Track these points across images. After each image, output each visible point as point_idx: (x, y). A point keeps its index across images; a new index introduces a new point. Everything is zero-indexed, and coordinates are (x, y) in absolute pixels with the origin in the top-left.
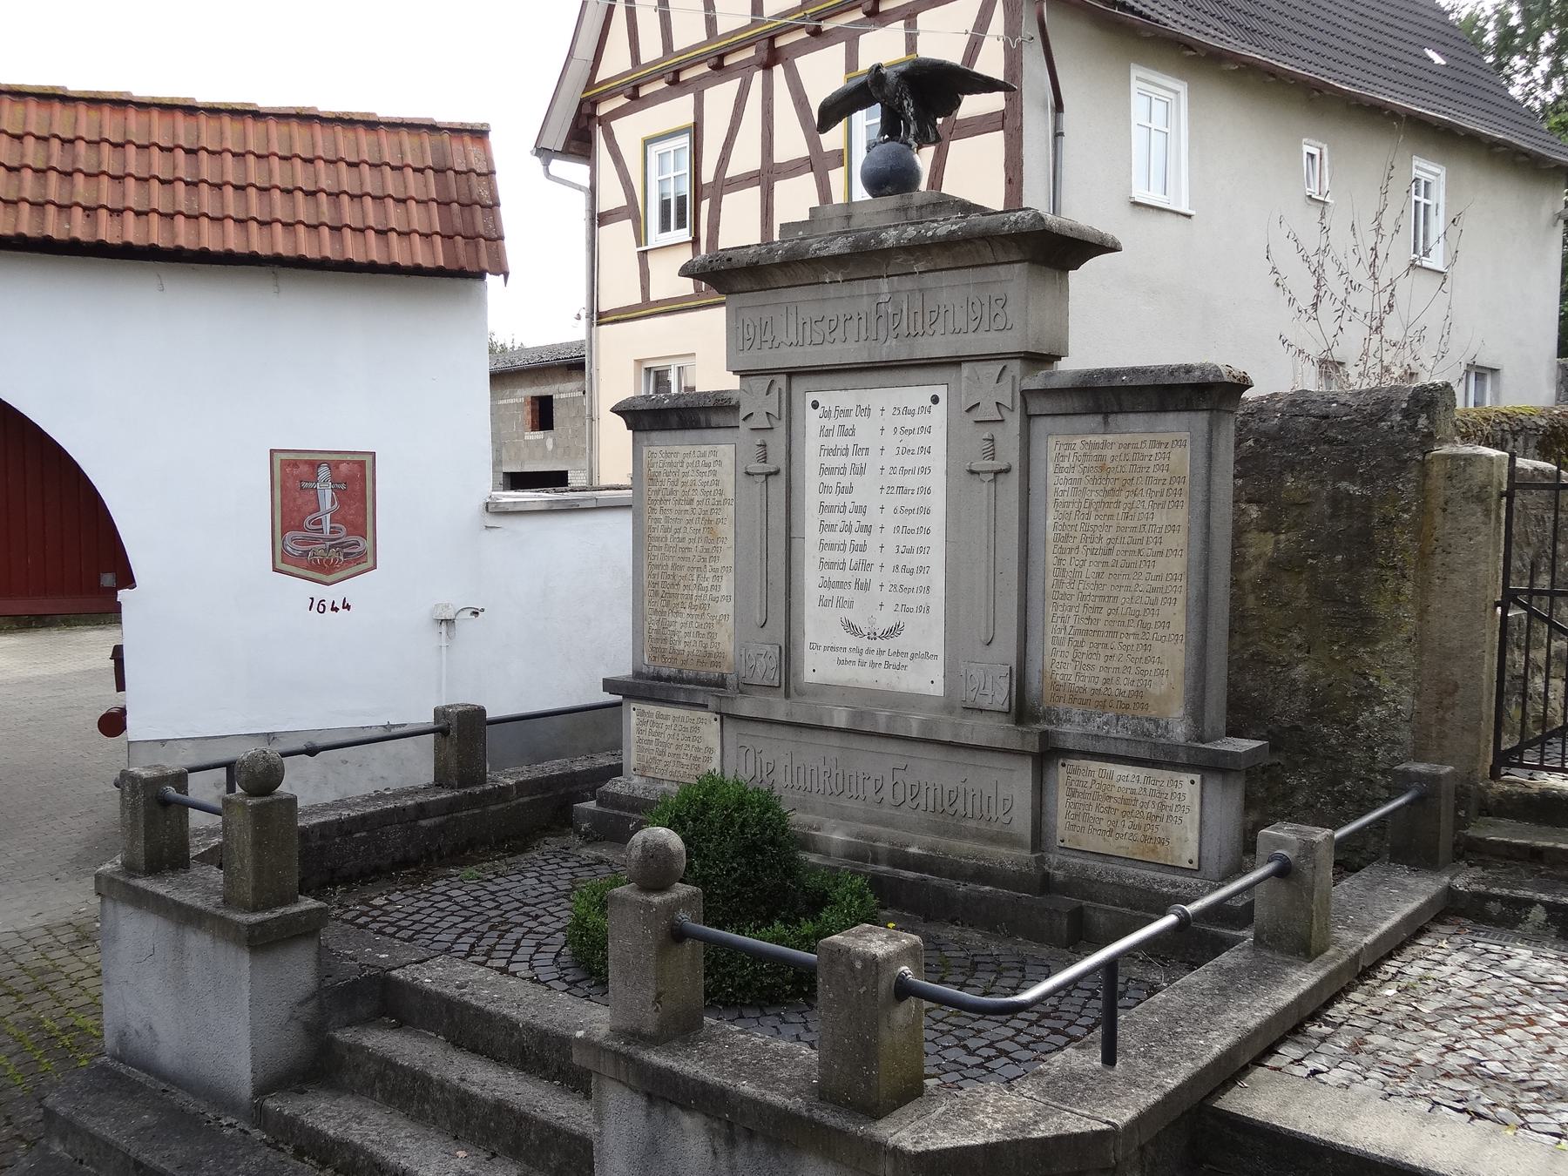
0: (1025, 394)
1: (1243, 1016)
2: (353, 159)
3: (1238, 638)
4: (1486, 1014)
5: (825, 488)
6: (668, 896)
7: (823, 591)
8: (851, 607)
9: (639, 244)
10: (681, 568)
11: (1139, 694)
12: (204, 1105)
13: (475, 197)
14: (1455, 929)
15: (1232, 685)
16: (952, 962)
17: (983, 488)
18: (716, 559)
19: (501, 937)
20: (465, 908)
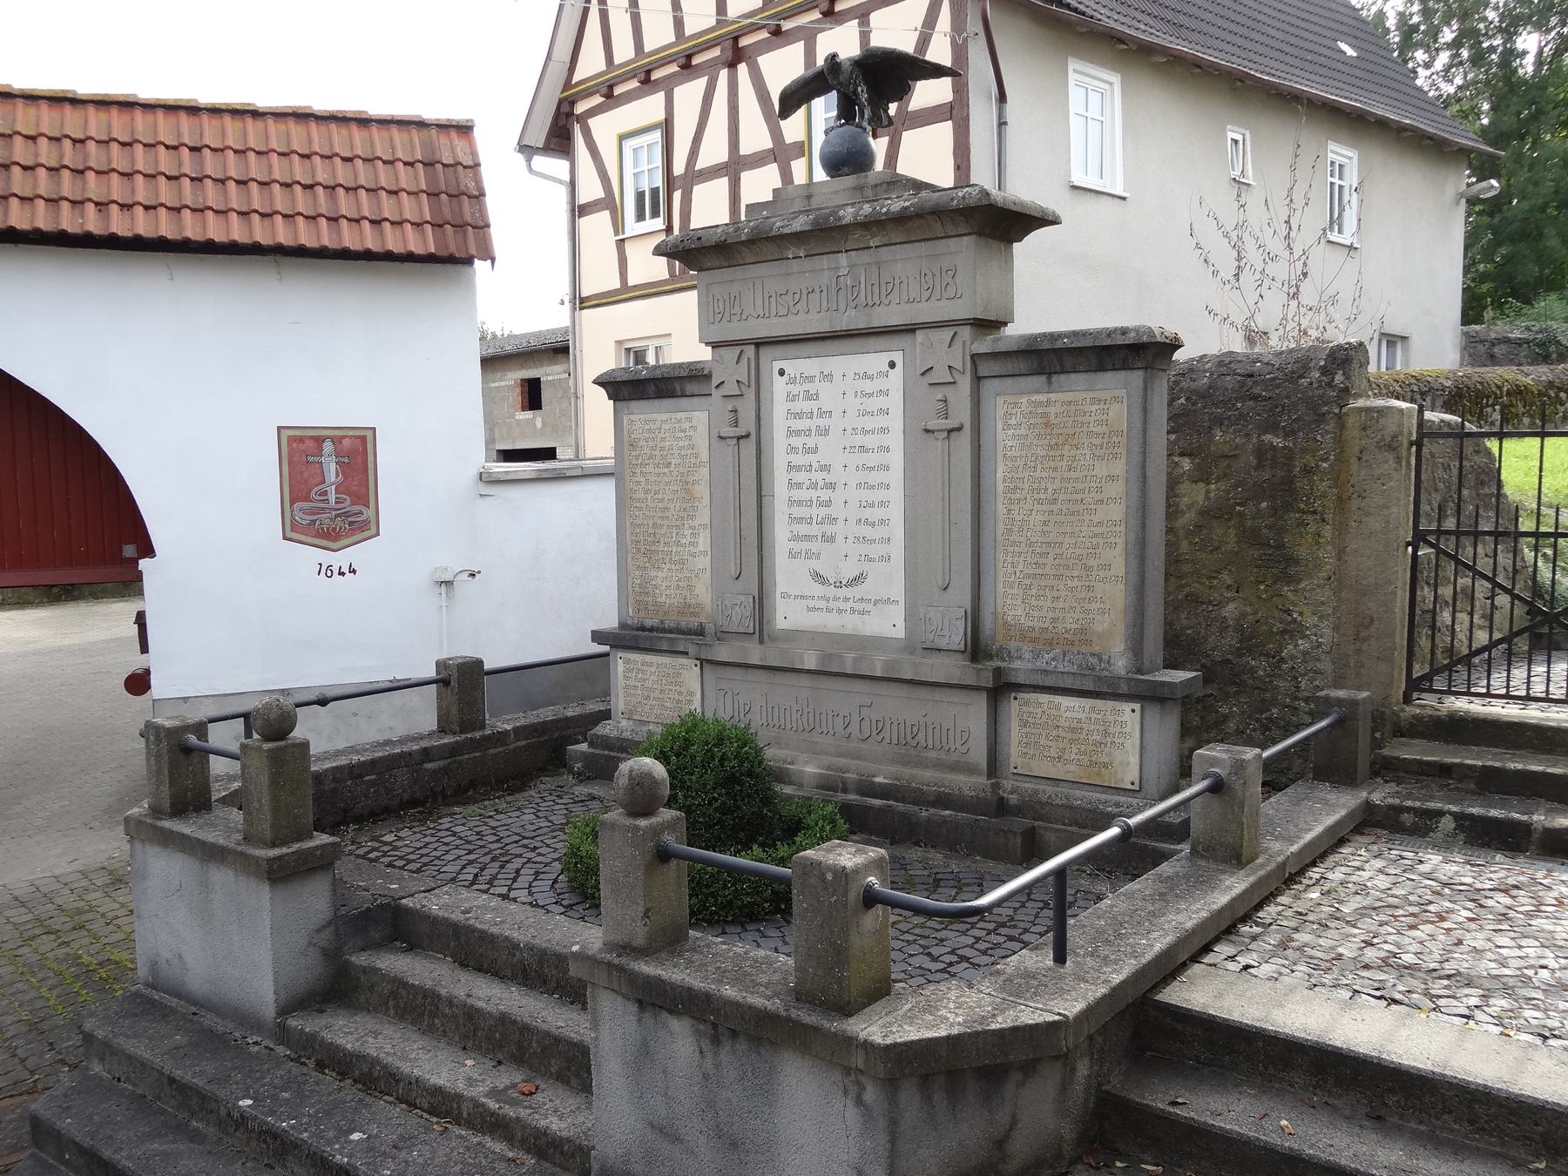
0: (975, 358)
1: (1180, 918)
2: (348, 155)
3: (1172, 580)
4: (1401, 912)
5: (792, 450)
6: (653, 820)
7: (793, 545)
8: (818, 558)
9: (617, 233)
11: (1083, 631)
12: (231, 1025)
13: (462, 188)
14: (1373, 839)
15: (1168, 624)
16: (917, 880)
17: (937, 445)
18: (692, 517)
19: (502, 867)
20: (468, 842)
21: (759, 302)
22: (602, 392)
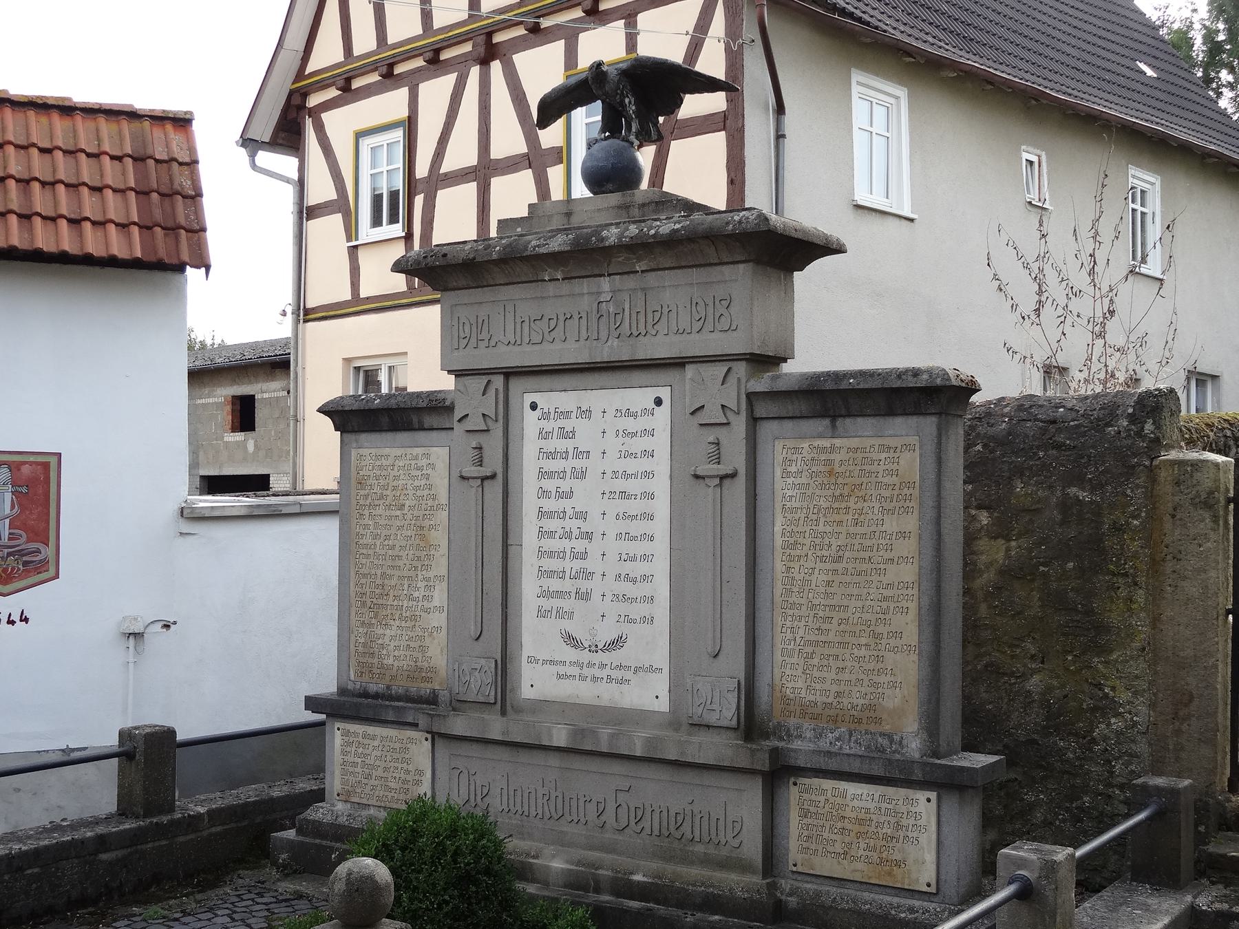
0: (751, 397)
5: (544, 493)
7: (542, 601)
9: (349, 239)
10: (391, 576)
11: (871, 707)
13: (176, 187)
15: (966, 698)
17: (707, 493)
21: (510, 327)
22: (328, 422)
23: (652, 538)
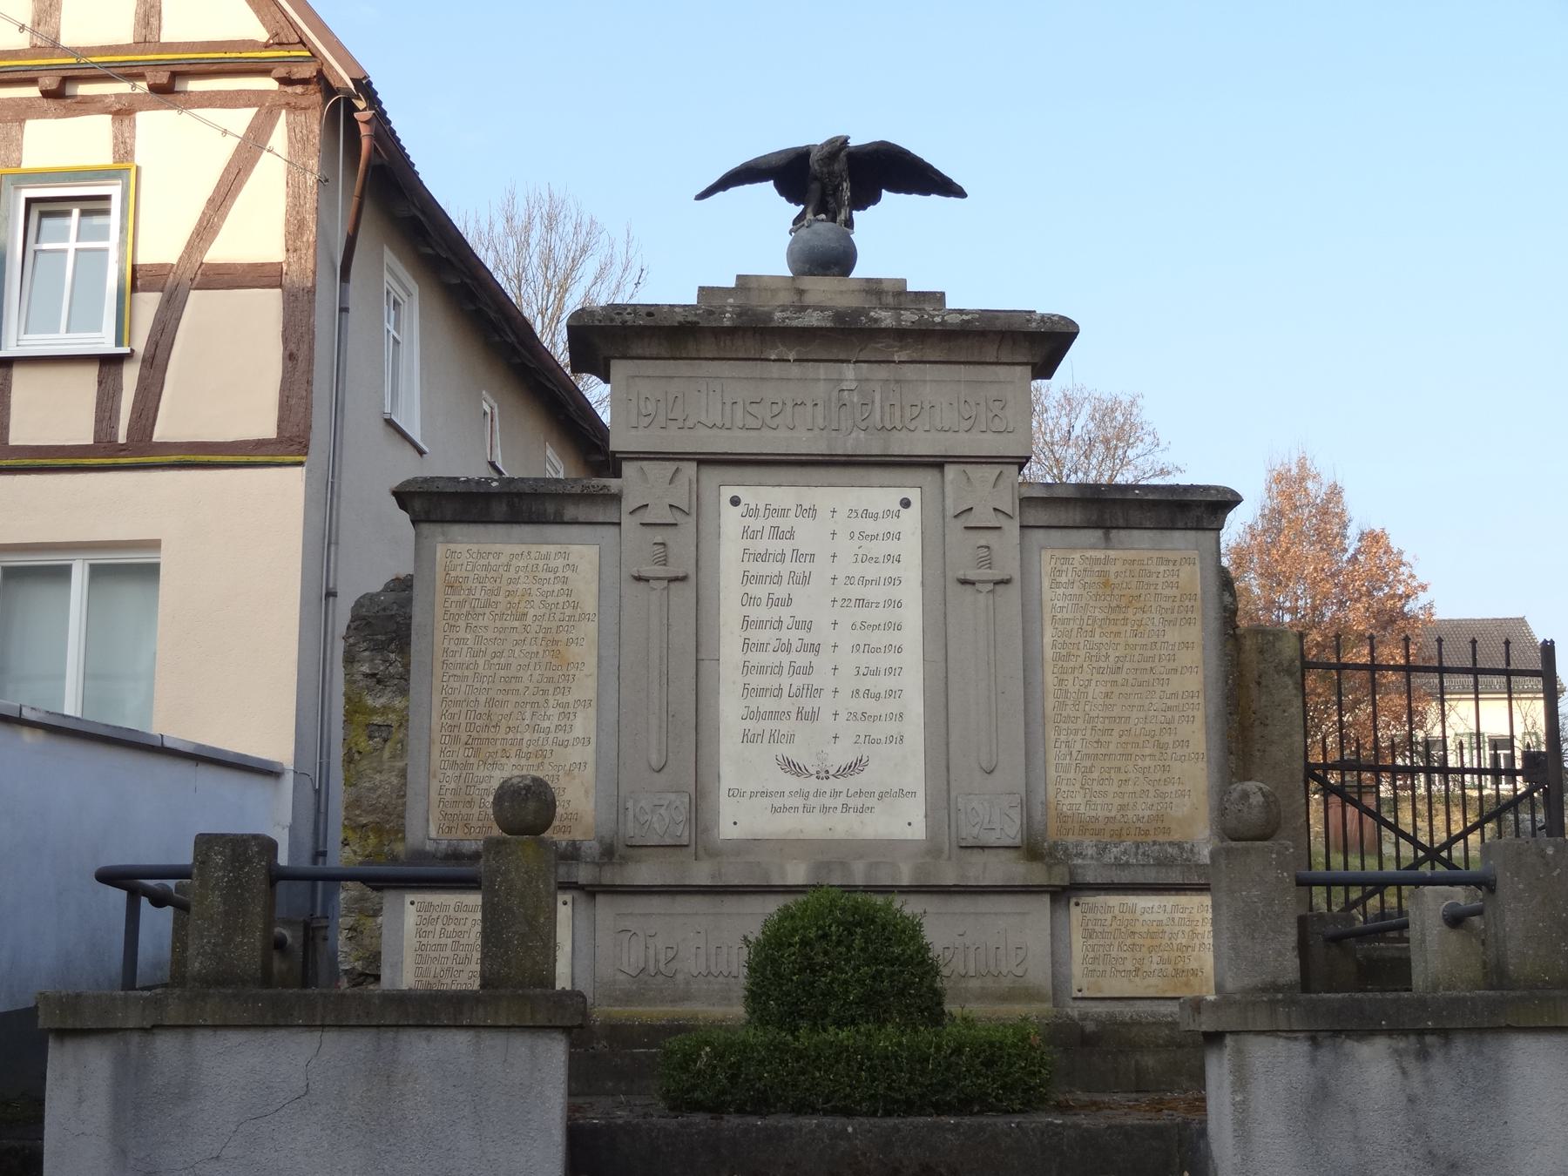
5: (749, 600)
7: (748, 724)
10: (503, 703)
11: (1159, 818)
23: (899, 650)
